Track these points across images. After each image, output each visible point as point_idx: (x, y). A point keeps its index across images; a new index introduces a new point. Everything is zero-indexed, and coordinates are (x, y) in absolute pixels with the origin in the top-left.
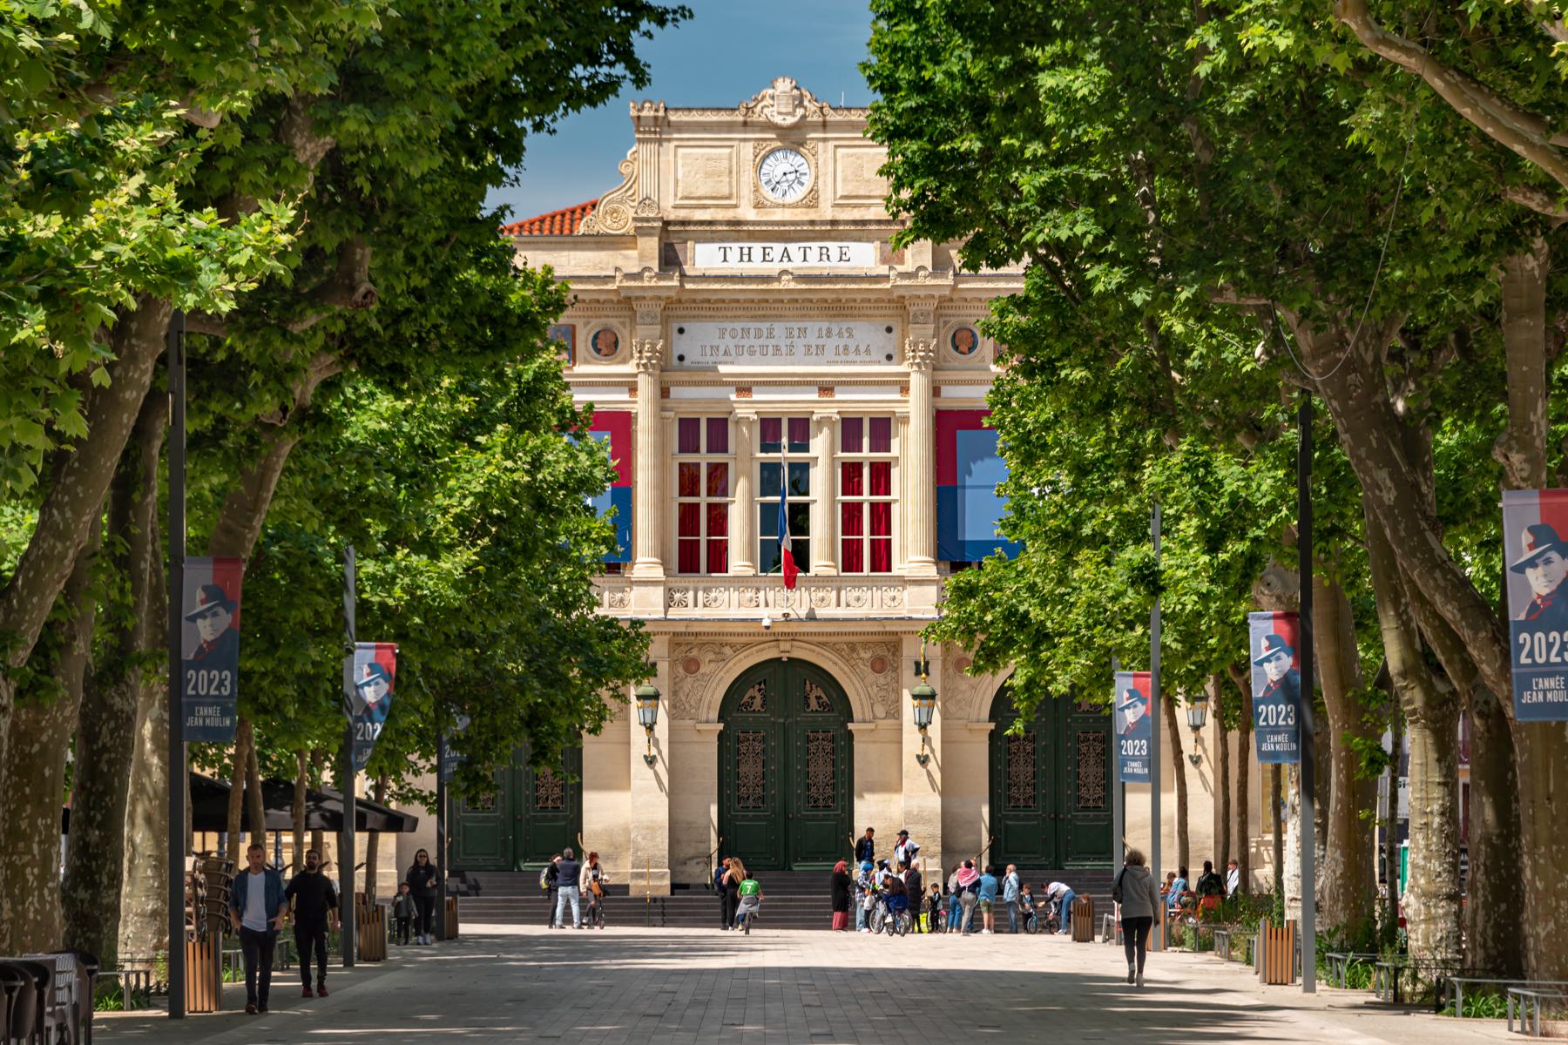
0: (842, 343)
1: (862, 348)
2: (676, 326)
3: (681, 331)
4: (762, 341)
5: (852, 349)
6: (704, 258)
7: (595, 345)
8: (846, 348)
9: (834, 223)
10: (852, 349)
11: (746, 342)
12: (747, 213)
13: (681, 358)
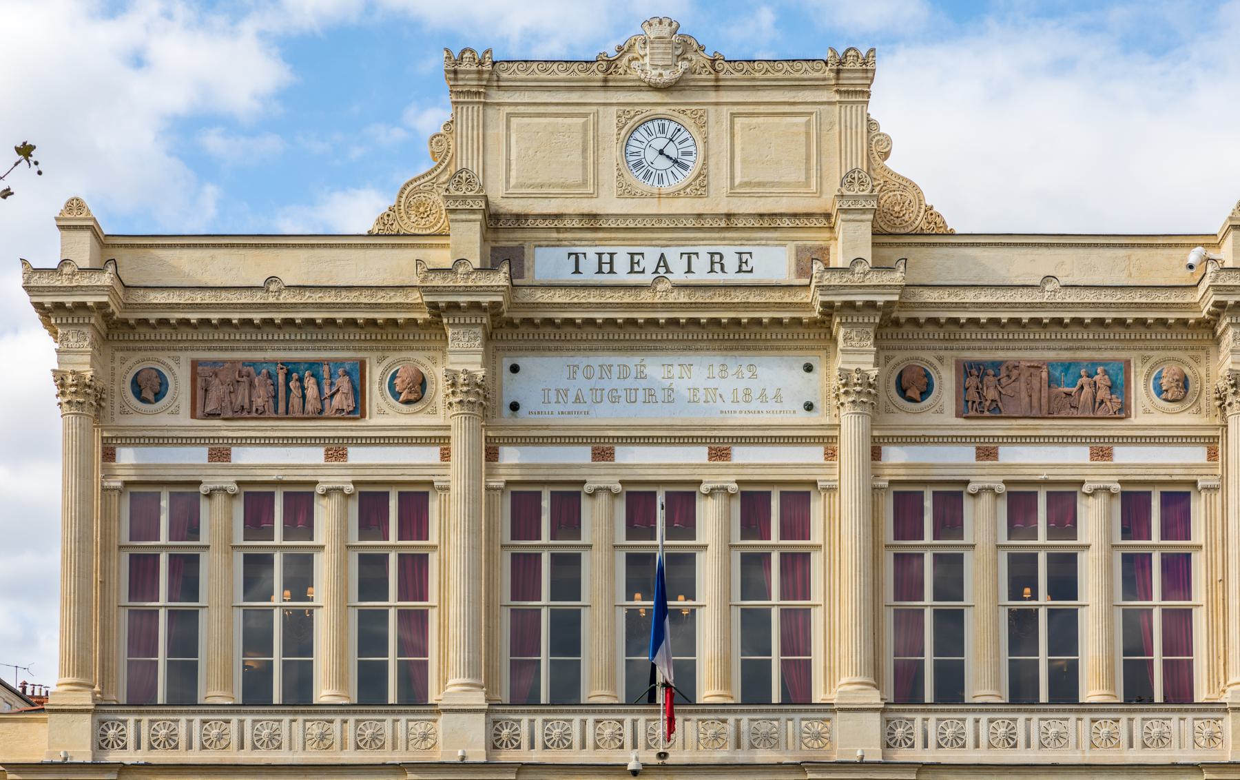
0: (741, 385)
1: (770, 393)
2: (507, 363)
3: (515, 369)
4: (630, 383)
5: (756, 394)
6: (548, 263)
7: (392, 386)
8: (747, 392)
9: (729, 216)
10: (756, 394)
11: (607, 385)
12: (607, 203)
13: (515, 407)
